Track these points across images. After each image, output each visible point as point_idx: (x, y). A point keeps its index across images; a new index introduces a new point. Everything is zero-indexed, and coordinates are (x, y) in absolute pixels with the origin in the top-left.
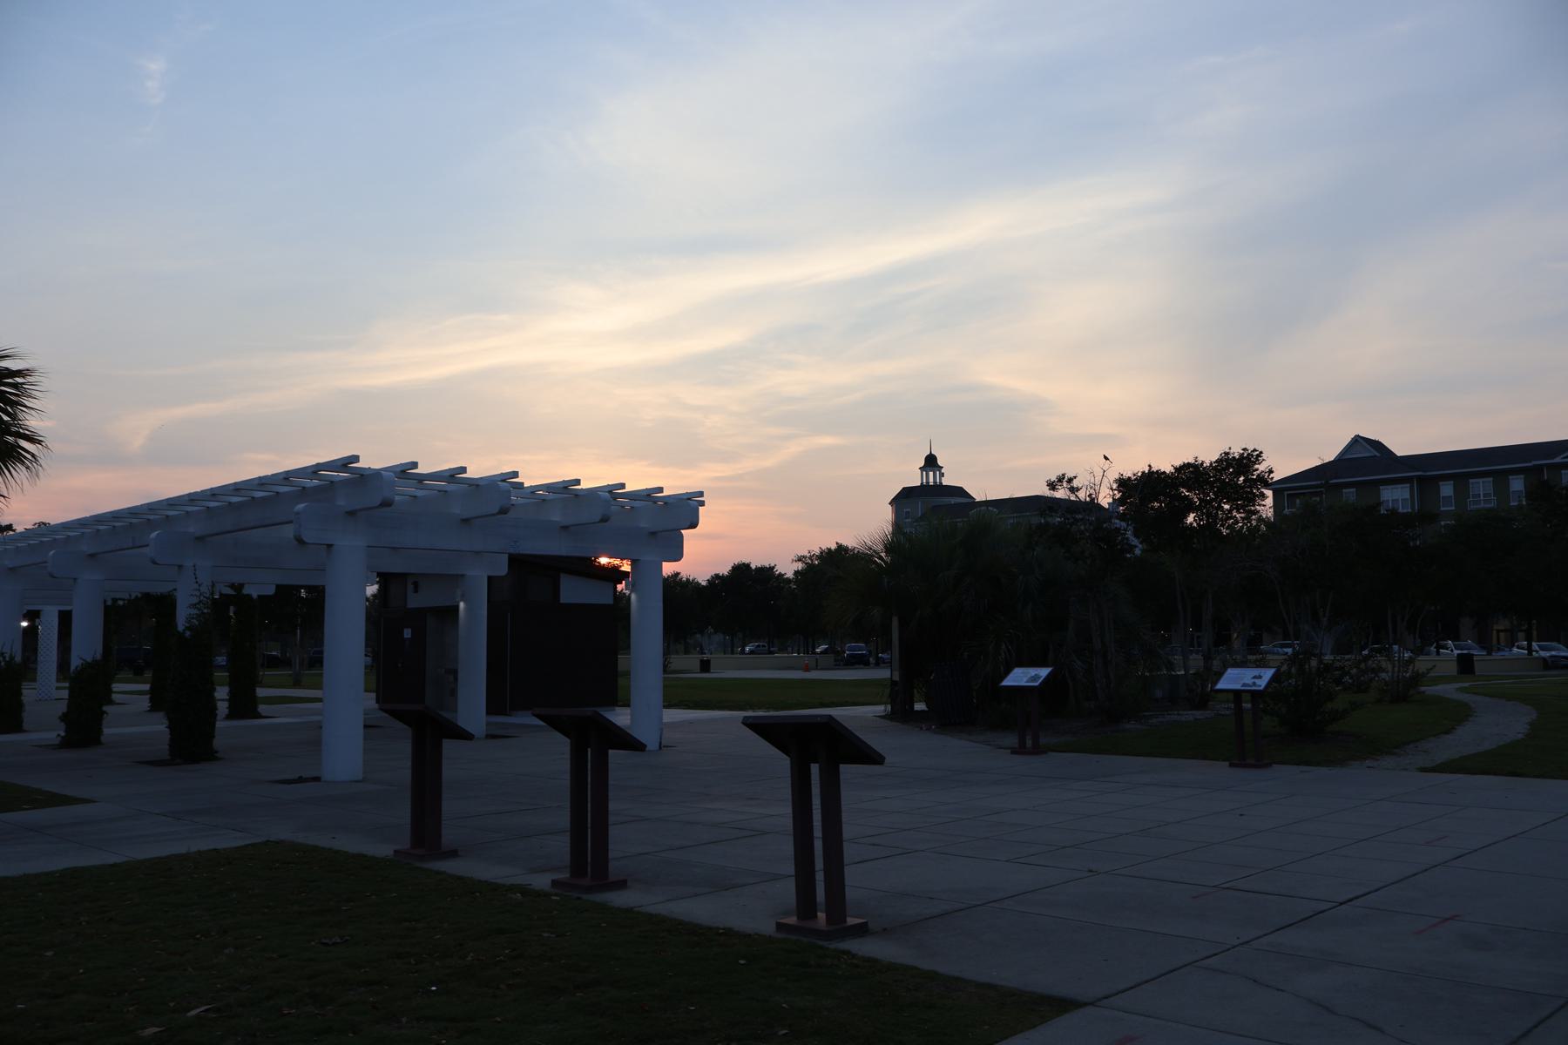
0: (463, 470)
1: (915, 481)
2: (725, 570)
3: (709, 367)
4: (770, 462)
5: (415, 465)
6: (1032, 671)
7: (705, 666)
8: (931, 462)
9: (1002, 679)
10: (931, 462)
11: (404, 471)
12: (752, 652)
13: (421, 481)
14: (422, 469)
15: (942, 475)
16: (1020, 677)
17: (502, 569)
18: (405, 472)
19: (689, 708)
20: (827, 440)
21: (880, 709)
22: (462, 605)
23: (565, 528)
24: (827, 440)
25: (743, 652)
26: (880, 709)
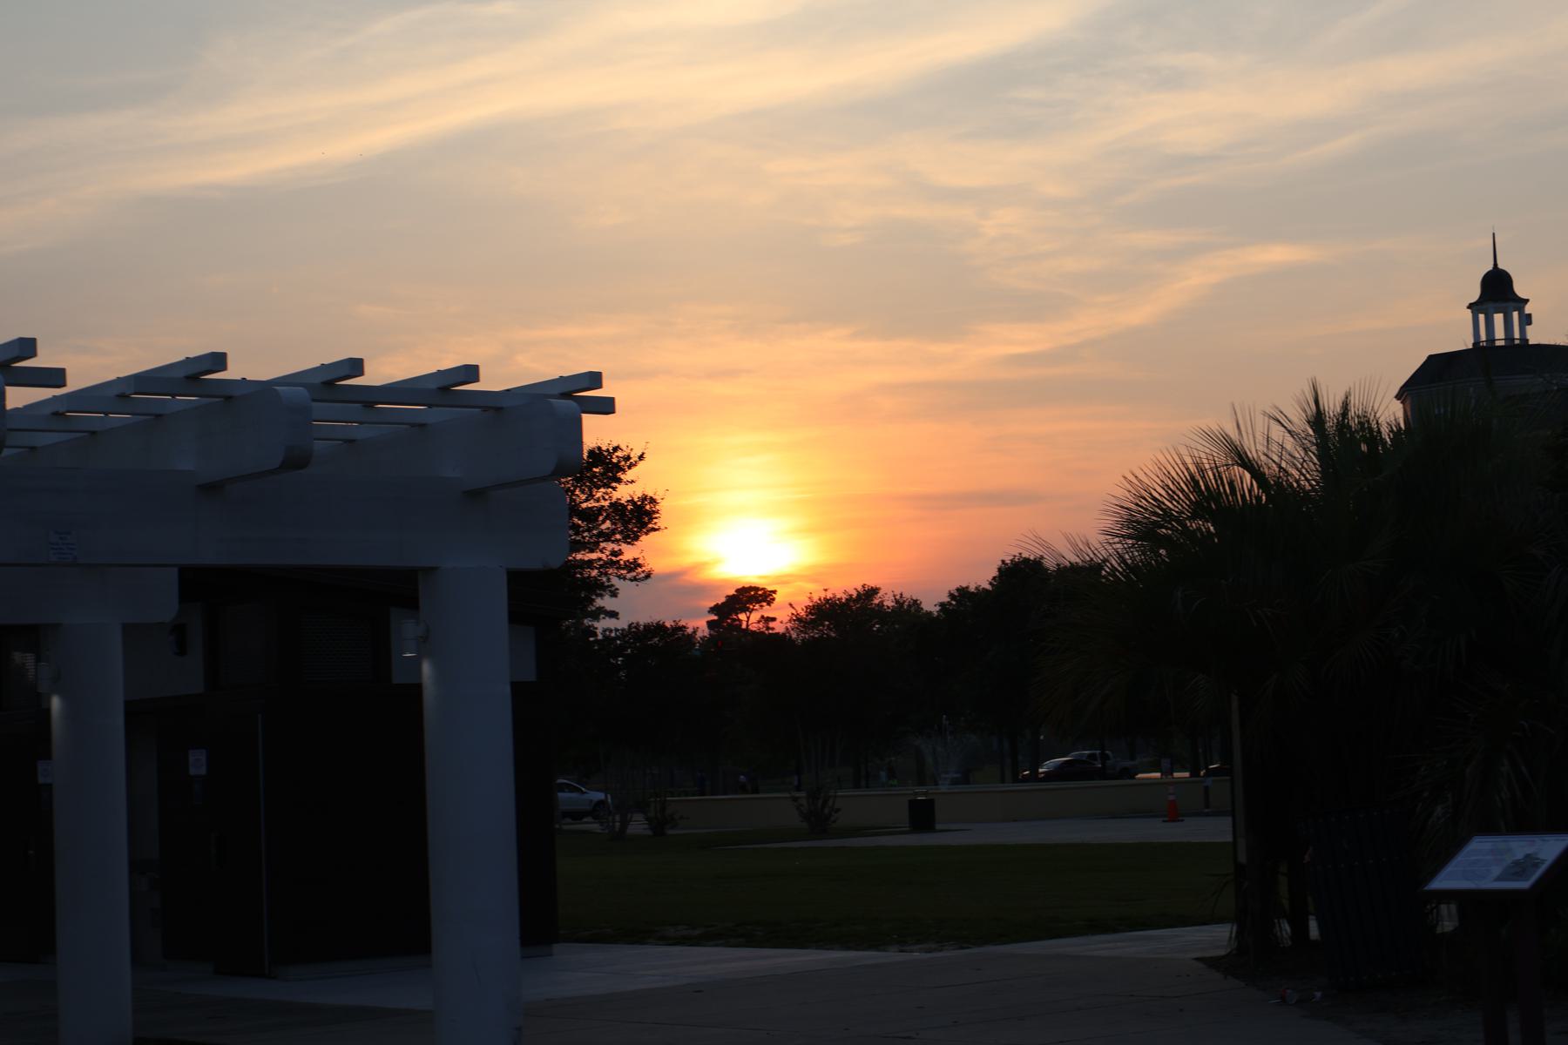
0: (471, 372)
1: (1457, 334)
2: (981, 577)
3: (983, 95)
4: (1139, 313)
5: (356, 366)
6: (1519, 847)
7: (922, 817)
8: (1497, 290)
9: (1434, 873)
10: (1497, 290)
11: (330, 384)
12: (1049, 777)
13: (369, 405)
14: (378, 373)
15: (1527, 320)
16: (1486, 863)
17: (164, 605)
18: (334, 384)
19: (750, 941)
20: (1277, 254)
21: (1218, 937)
22: (56, 703)
23: (211, 489)
24: (1277, 254)
25: (1034, 777)
26: (1218, 937)
